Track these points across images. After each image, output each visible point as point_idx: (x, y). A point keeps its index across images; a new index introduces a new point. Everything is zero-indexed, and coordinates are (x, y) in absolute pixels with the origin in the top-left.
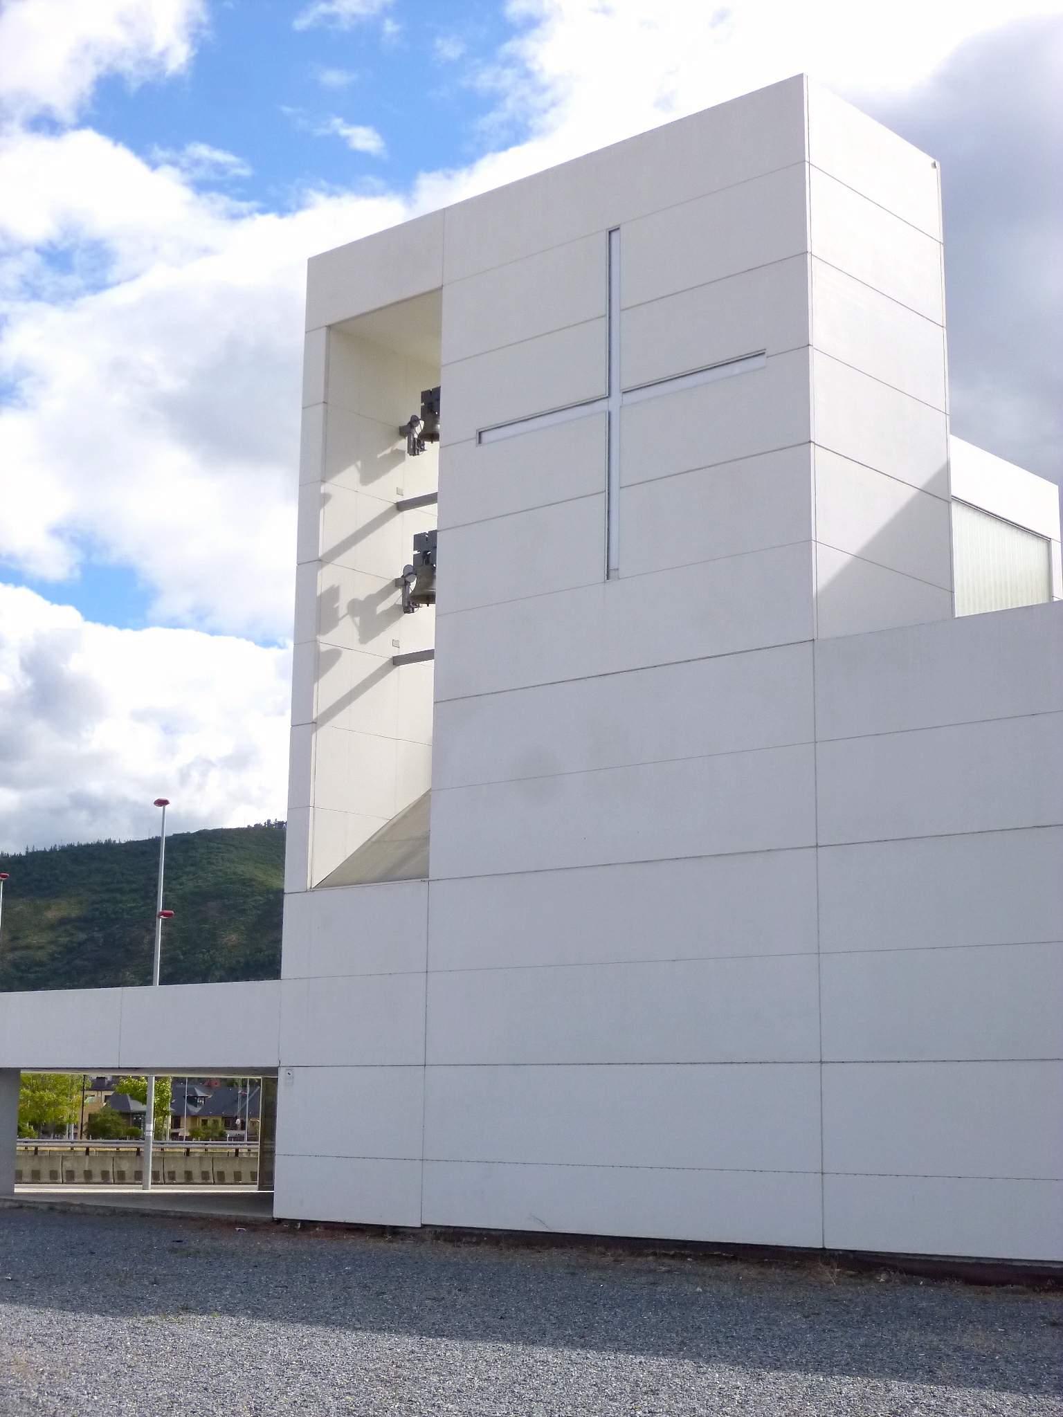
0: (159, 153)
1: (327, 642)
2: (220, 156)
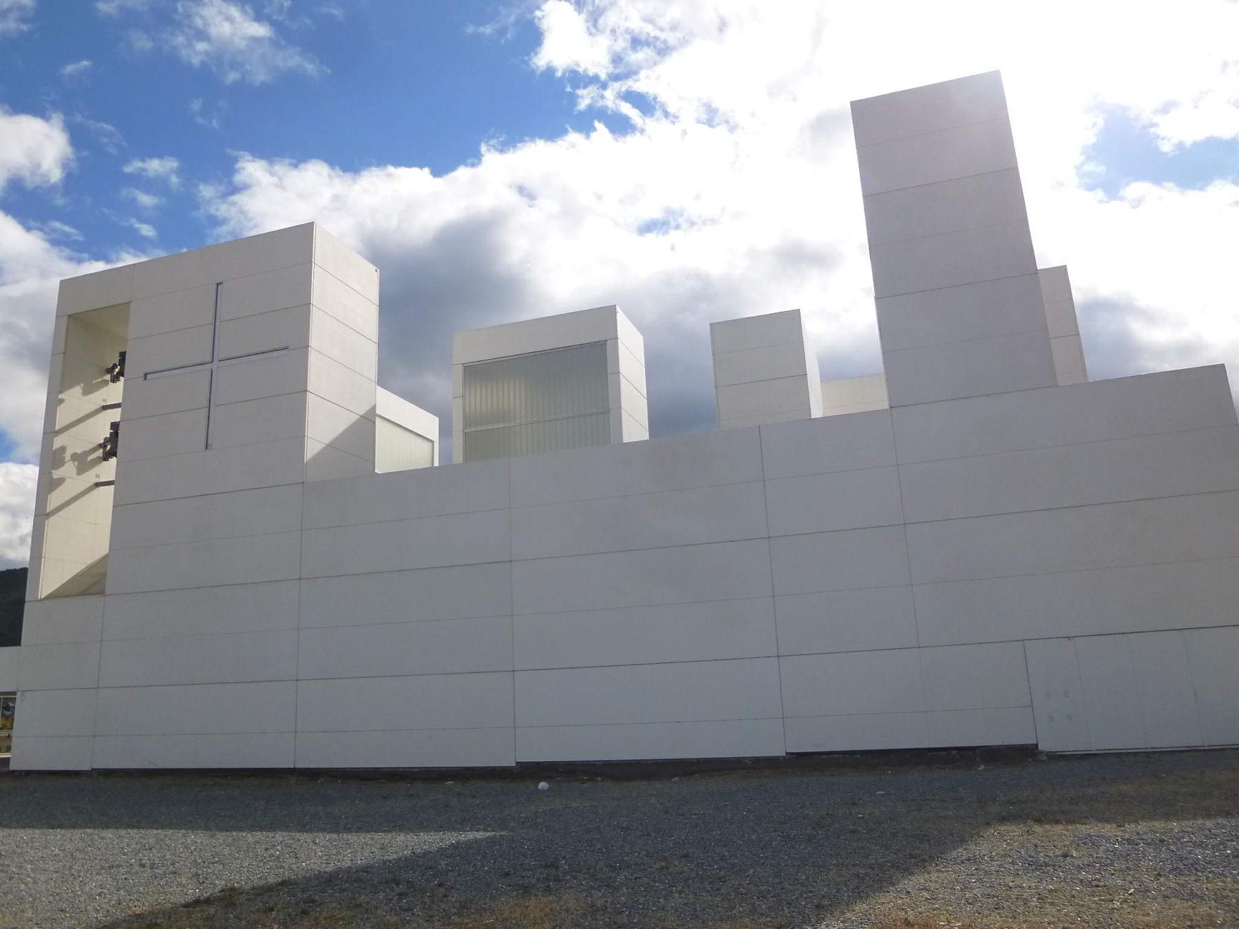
0: (32, 223)
1: (56, 474)
2: (67, 228)
